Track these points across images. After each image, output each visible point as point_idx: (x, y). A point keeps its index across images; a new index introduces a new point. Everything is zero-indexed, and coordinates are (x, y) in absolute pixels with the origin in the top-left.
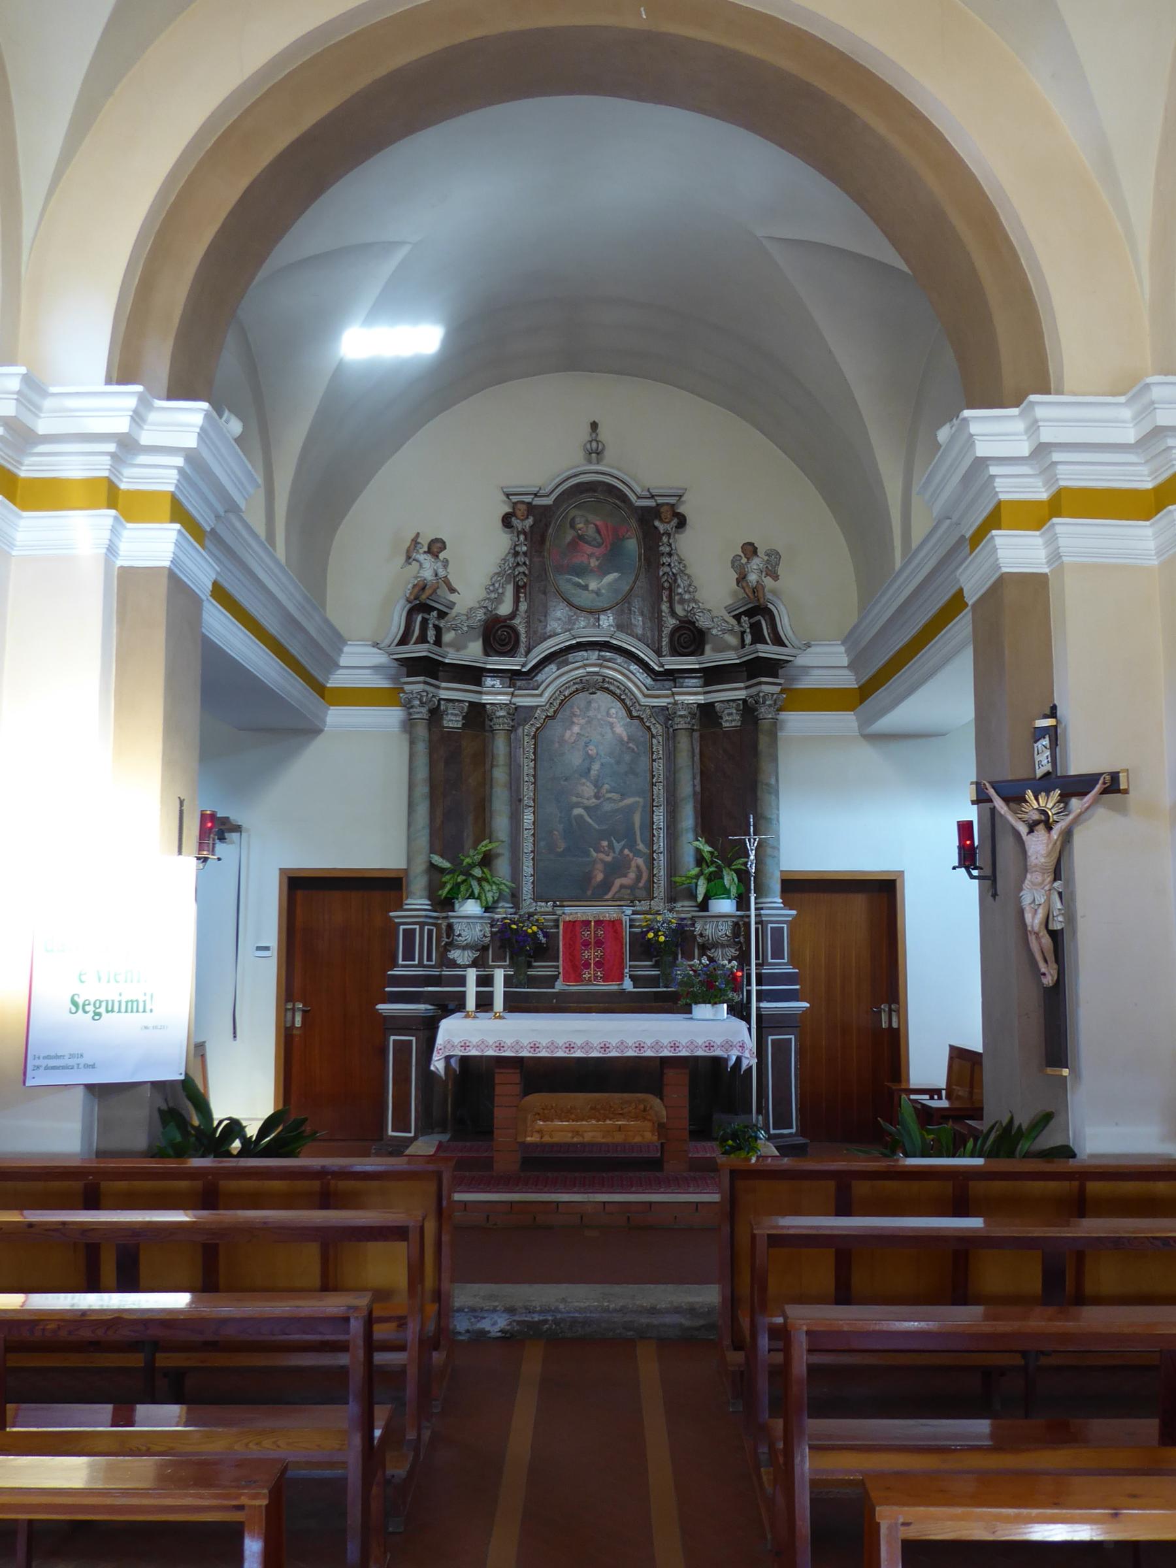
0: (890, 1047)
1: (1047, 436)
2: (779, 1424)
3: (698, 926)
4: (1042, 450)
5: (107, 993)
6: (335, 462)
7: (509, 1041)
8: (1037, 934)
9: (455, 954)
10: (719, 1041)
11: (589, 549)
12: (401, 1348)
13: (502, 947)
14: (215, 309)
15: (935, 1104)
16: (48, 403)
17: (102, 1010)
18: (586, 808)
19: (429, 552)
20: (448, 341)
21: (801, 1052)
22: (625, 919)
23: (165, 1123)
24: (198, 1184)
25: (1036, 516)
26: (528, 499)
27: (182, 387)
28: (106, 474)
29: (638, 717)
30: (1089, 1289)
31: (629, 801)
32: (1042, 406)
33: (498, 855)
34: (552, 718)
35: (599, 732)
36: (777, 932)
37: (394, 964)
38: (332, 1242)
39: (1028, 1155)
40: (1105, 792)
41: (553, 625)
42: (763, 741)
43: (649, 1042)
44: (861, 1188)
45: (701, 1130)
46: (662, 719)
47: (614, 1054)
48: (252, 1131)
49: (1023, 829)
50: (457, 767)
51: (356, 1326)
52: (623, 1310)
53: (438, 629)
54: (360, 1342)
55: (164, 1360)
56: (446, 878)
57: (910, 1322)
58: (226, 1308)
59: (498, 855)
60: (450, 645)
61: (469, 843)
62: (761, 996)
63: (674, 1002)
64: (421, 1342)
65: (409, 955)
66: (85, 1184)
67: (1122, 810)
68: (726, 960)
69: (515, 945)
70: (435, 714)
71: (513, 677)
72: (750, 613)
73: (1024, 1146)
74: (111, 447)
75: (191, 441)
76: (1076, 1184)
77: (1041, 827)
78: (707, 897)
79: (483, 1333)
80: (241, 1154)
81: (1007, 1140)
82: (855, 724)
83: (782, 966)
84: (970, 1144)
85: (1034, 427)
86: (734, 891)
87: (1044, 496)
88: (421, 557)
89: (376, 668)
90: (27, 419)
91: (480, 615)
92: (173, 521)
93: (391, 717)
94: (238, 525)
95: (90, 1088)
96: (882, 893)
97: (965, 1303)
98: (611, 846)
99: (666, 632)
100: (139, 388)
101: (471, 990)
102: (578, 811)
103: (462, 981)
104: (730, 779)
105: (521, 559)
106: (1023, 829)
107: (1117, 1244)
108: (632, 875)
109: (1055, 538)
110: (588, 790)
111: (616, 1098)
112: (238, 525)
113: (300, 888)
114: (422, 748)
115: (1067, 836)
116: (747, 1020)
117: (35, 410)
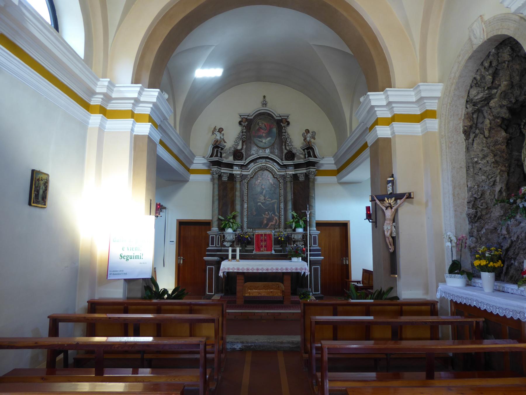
0: (346, 269)
1: (391, 99)
2: (319, 374)
3: (293, 236)
4: (389, 103)
5: (130, 253)
6: (193, 105)
7: (241, 268)
8: (388, 238)
9: (225, 243)
10: (299, 268)
11: (263, 131)
12: (213, 353)
13: (238, 241)
14: (161, 64)
15: (359, 285)
16: (115, 89)
17: (129, 258)
18: (262, 203)
19: (219, 131)
20: (224, 73)
21: (321, 271)
22: (273, 234)
23: (146, 290)
24: (156, 307)
25: (388, 122)
26: (246, 117)
27: (152, 85)
28: (131, 109)
29: (276, 178)
30: (404, 336)
31: (273, 201)
32: (390, 91)
33: (237, 216)
34: (252, 178)
35: (265, 181)
36: (315, 238)
37: (208, 246)
38: (193, 325)
39: (386, 299)
40: (407, 198)
41: (253, 152)
42: (311, 184)
43: (280, 268)
44: (340, 308)
45: (294, 292)
46: (283, 178)
47: (270, 271)
48: (170, 292)
49: (384, 208)
50: (226, 192)
51: (202, 347)
52: (274, 342)
53: (221, 153)
54: (203, 351)
55: (146, 356)
56: (223, 222)
57: (354, 345)
58: (165, 341)
59: (237, 216)
60: (224, 157)
61: (229, 213)
62: (311, 255)
63: (287, 257)
64: (218, 351)
65: (212, 244)
66: (124, 306)
67: (412, 203)
68: (301, 245)
69: (242, 241)
70: (220, 177)
71: (241, 166)
72: (307, 149)
73: (385, 296)
74: (133, 101)
75: (155, 100)
76: (399, 307)
77: (389, 208)
78: (295, 228)
79: (235, 349)
80: (167, 298)
81: (380, 295)
82: (336, 180)
83: (316, 247)
84: (370, 296)
85: (387, 97)
86: (303, 226)
87: (390, 116)
88: (217, 133)
89: (204, 164)
90: (110, 93)
91: (233, 149)
92: (149, 122)
93: (208, 177)
94: (167, 124)
95: (125, 280)
96: (344, 227)
97: (369, 340)
98: (268, 213)
99: (284, 154)
100: (140, 85)
101: (230, 253)
102: (259, 204)
103: (228, 251)
104: (302, 195)
105: (244, 134)
106: (384, 208)
107: (412, 323)
108: (274, 221)
109: (393, 128)
110: (262, 198)
111: (270, 283)
112: (167, 124)
113: (182, 225)
114: (216, 186)
115: (397, 210)
116: (307, 262)
117: (112, 91)
